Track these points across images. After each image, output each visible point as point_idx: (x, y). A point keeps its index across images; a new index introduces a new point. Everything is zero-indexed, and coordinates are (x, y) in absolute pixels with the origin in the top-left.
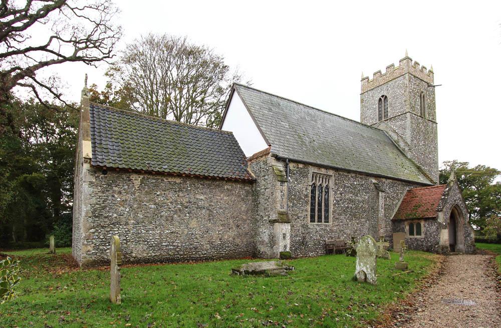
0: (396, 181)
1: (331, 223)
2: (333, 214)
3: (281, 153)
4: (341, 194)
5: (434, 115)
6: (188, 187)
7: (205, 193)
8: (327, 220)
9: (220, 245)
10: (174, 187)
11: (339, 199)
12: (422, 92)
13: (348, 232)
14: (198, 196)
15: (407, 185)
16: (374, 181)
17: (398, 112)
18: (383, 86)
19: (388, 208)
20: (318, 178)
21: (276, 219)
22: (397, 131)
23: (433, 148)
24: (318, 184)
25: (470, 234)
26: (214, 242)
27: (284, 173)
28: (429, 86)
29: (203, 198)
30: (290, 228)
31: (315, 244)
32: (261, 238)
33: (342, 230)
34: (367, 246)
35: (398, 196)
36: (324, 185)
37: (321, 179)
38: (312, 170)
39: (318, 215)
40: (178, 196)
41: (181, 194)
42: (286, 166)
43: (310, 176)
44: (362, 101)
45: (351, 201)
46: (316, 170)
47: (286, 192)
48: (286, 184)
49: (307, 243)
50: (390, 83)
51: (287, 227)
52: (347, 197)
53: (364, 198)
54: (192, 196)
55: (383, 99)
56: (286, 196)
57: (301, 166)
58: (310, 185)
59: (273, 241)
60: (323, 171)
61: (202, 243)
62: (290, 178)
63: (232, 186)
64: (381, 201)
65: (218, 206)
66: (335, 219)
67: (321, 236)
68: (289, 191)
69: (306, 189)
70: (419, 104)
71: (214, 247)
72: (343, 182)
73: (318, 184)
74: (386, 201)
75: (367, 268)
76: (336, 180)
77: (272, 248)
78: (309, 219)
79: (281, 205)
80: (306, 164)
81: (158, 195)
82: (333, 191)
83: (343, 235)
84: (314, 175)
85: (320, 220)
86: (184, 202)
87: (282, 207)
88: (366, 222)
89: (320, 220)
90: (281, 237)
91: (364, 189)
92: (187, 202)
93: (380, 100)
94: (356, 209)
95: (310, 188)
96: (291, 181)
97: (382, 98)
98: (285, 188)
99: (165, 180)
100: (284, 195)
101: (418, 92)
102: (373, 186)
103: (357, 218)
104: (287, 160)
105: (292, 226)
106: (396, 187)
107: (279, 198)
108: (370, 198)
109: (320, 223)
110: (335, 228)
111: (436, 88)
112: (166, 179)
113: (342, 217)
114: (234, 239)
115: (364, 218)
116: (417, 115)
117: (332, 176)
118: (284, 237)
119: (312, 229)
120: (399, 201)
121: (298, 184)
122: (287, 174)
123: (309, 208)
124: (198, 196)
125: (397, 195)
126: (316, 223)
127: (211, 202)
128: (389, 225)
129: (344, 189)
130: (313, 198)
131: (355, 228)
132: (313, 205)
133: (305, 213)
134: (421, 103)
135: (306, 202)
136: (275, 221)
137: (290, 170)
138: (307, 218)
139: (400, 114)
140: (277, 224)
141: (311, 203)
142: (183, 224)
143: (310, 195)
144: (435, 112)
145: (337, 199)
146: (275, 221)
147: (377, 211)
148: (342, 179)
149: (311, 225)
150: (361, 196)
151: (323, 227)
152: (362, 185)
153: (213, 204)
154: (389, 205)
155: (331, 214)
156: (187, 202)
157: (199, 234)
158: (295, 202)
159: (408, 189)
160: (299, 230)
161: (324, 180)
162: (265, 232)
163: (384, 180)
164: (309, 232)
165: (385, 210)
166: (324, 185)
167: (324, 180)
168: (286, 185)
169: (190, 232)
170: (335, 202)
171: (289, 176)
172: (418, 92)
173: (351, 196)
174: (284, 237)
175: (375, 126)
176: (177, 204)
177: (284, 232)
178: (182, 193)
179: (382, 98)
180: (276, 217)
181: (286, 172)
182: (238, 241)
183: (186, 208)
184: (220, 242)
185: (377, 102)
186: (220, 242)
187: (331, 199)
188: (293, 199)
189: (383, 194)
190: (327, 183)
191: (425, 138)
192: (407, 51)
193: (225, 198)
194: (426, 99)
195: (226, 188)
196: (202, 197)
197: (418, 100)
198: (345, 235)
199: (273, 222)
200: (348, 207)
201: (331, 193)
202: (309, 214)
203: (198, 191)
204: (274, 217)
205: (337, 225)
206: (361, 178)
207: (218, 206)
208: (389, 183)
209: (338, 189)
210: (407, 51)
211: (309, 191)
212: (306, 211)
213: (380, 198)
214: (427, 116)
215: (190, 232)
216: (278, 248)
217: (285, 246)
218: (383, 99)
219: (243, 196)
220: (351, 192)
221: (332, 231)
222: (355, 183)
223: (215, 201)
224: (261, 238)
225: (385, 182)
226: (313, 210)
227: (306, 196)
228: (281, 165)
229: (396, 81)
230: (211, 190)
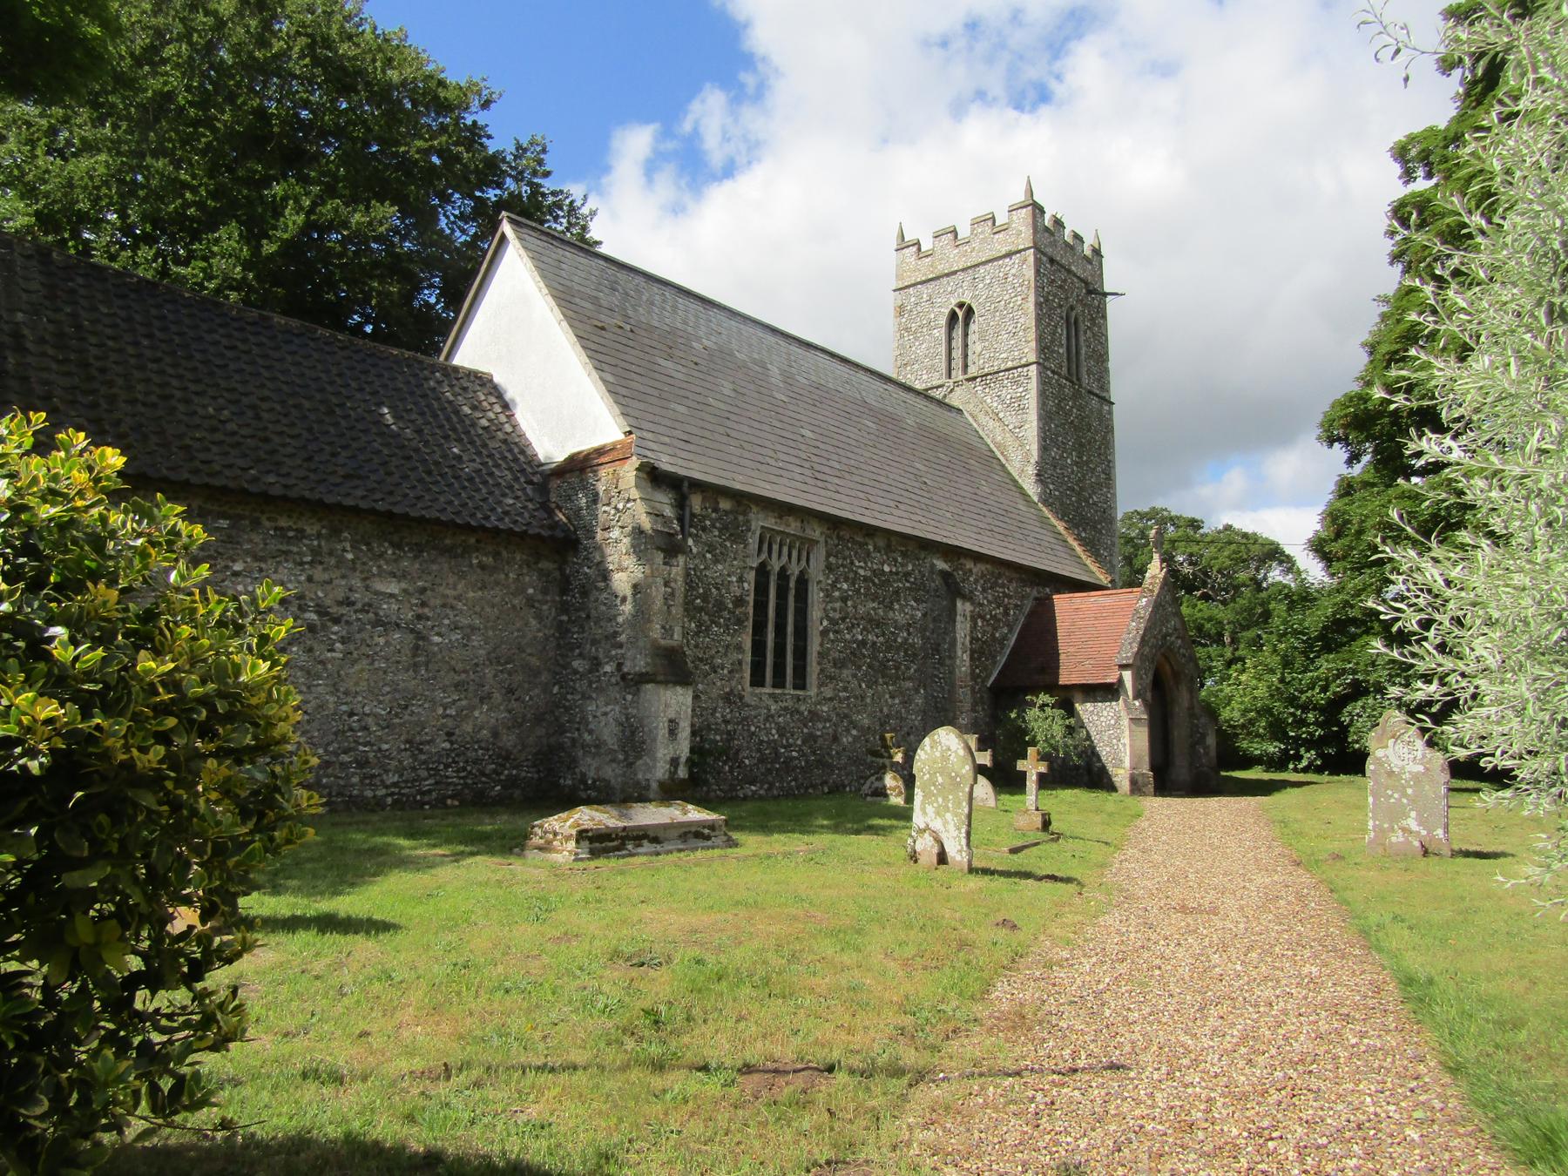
0: (1002, 570)
1: (812, 691)
2: (819, 663)
3: (665, 458)
4: (844, 599)
5: (1104, 386)
6: (344, 550)
7: (402, 576)
8: (801, 683)
9: (448, 756)
10: (295, 549)
11: (837, 616)
12: (1072, 308)
13: (864, 720)
14: (379, 586)
15: (1032, 584)
16: (941, 565)
17: (1004, 359)
18: (961, 276)
19: (981, 652)
20: (775, 547)
21: (648, 669)
22: (1001, 415)
23: (1103, 476)
24: (775, 565)
25: (1204, 736)
26: (428, 742)
27: (676, 526)
28: (1090, 292)
29: (396, 591)
30: (689, 700)
31: (762, 760)
32: (591, 732)
33: (846, 716)
34: (945, 758)
35: (1008, 614)
36: (794, 570)
37: (785, 550)
38: (760, 521)
39: (796, 627)
40: (310, 579)
41: (319, 574)
42: (681, 504)
43: (753, 541)
44: (901, 310)
45: (875, 623)
46: (771, 522)
47: (679, 586)
48: (681, 559)
49: (738, 751)
50: (982, 270)
51: (681, 699)
52: (861, 610)
53: (912, 616)
54: (356, 582)
55: (960, 314)
56: (679, 598)
57: (725, 505)
58: (751, 568)
59: (634, 742)
60: (793, 527)
61: (385, 747)
62: (690, 542)
63: (496, 555)
64: (962, 630)
65: (446, 622)
66: (826, 678)
67: (782, 731)
68: (690, 583)
69: (741, 580)
70: (1064, 342)
71: (424, 762)
72: (852, 563)
73: (775, 565)
74: (974, 626)
75: (945, 823)
76: (828, 555)
77: (630, 765)
78: (747, 675)
79: (663, 627)
80: (744, 500)
81: (236, 574)
82: (821, 589)
83: (848, 730)
84: (766, 540)
85: (779, 682)
86: (328, 602)
87: (667, 631)
88: (917, 691)
89: (779, 682)
90: (663, 732)
91: (909, 589)
92: (340, 603)
93: (953, 317)
94: (889, 649)
95: (751, 576)
96: (695, 550)
97: (957, 310)
98: (677, 574)
99: (267, 524)
100: (672, 594)
101: (1060, 306)
102: (938, 581)
103: (891, 679)
104: (686, 484)
105: (696, 697)
106: (1003, 586)
107: (659, 603)
108: (929, 618)
109: (778, 691)
110: (825, 709)
111: (1109, 298)
112: (269, 519)
113: (846, 673)
114: (495, 734)
115: (910, 678)
116: (1059, 375)
117: (818, 542)
118: (673, 732)
119: (756, 707)
120: (1011, 630)
121: (716, 561)
122: (682, 527)
123: (747, 641)
124: (379, 586)
125: (1006, 613)
126: (768, 690)
127: (423, 604)
128: (983, 703)
129: (853, 584)
130: (761, 606)
131: (885, 710)
132: (759, 628)
133: (736, 656)
134: (1068, 338)
135: (740, 622)
136: (643, 679)
137: (693, 515)
138: (741, 670)
139: (1010, 364)
140: (649, 686)
141: (756, 602)
142: (320, 678)
143: (751, 599)
144: (1107, 370)
145: (831, 614)
146: (643, 679)
147: (950, 657)
148: (847, 553)
149: (752, 694)
150: (902, 610)
151: (790, 704)
152: (907, 574)
153: (430, 615)
154: (984, 642)
155: (814, 664)
156: (340, 603)
157: (376, 716)
158: (706, 618)
159: (1035, 593)
160: (715, 710)
161: (795, 554)
162: (605, 714)
163: (969, 565)
164: (745, 719)
165: (972, 659)
166: (794, 570)
167: (795, 554)
168: (681, 563)
169: (344, 708)
170: (825, 623)
171: (691, 535)
172: (1060, 306)
173: (874, 609)
174: (673, 732)
175: (938, 394)
176: (303, 609)
177: (671, 714)
178: (325, 570)
179: (957, 310)
180: (648, 664)
181: (681, 520)
182: (509, 740)
183: (337, 621)
184: (447, 745)
185: (943, 321)
186: (447, 745)
187: (815, 613)
188: (701, 609)
189: (968, 607)
190: (803, 563)
191: (1082, 445)
192: (1029, 182)
193: (471, 594)
194: (1082, 327)
195: (475, 561)
196: (393, 587)
197: (1062, 331)
198: (854, 732)
199: (634, 682)
200: (863, 643)
201: (816, 596)
202: (748, 658)
203: (379, 567)
204: (638, 662)
205: (831, 699)
206: (904, 555)
207: (446, 622)
208: (983, 576)
209: (833, 586)
210: (1029, 182)
211: (749, 586)
212: (739, 648)
213: (959, 618)
214: (1085, 379)
215: (344, 708)
216: (649, 769)
217: (674, 762)
218: (960, 314)
219: (531, 591)
220: (875, 598)
221: (815, 716)
222: (887, 569)
223: (438, 602)
224: (591, 732)
225: (970, 570)
226: (758, 647)
227: (739, 601)
228: (667, 501)
229: (1000, 267)
230: (425, 566)
